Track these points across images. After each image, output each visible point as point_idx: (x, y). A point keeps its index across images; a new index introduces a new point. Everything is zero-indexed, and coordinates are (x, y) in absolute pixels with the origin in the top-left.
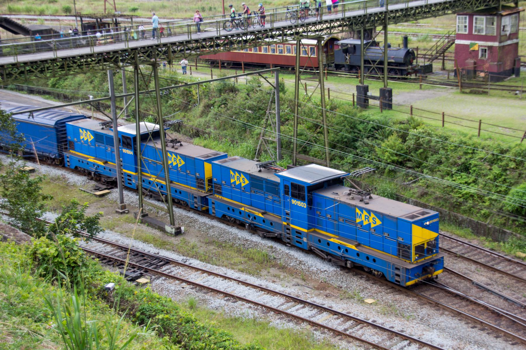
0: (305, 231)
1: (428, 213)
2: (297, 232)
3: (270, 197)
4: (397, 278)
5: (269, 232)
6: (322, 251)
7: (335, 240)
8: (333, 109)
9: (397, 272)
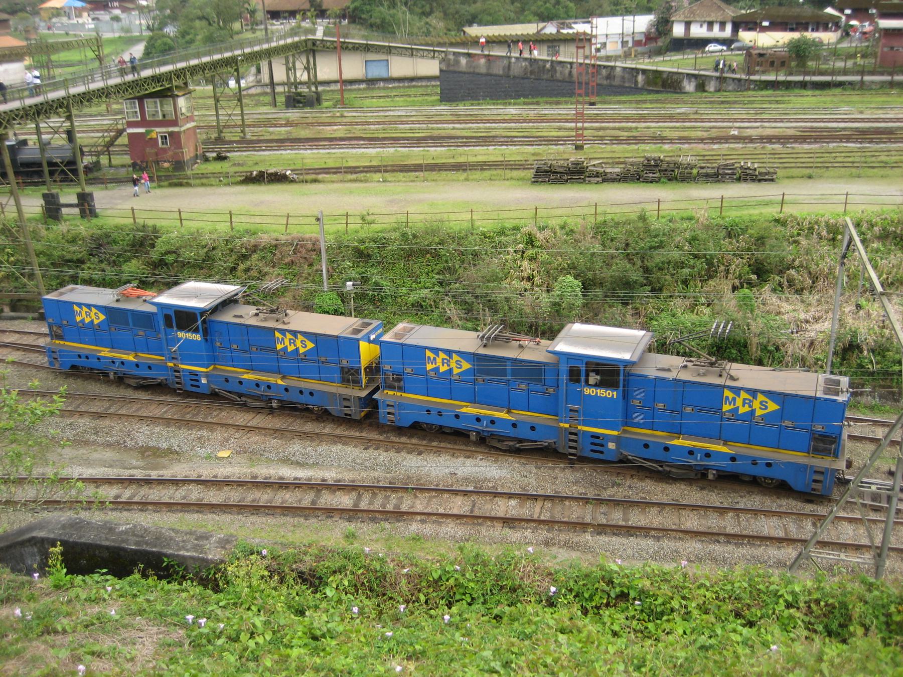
1: (370, 324)
2: (593, 437)
3: (141, 333)
4: (347, 411)
5: (145, 379)
6: (230, 392)
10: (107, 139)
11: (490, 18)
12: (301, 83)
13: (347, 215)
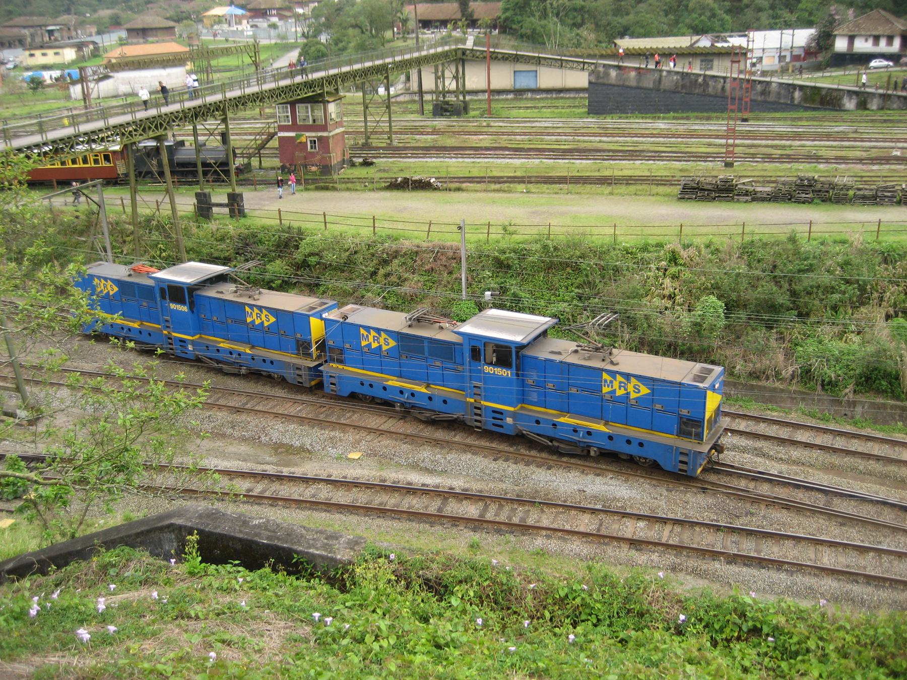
0: (511, 409)
1: (326, 304)
2: (494, 411)
4: (684, 467)
6: (211, 359)
7: (224, 345)
8: (556, 249)
9: (298, 372)
10: (259, 142)
11: (642, 31)
12: (449, 92)
13: (489, 225)
